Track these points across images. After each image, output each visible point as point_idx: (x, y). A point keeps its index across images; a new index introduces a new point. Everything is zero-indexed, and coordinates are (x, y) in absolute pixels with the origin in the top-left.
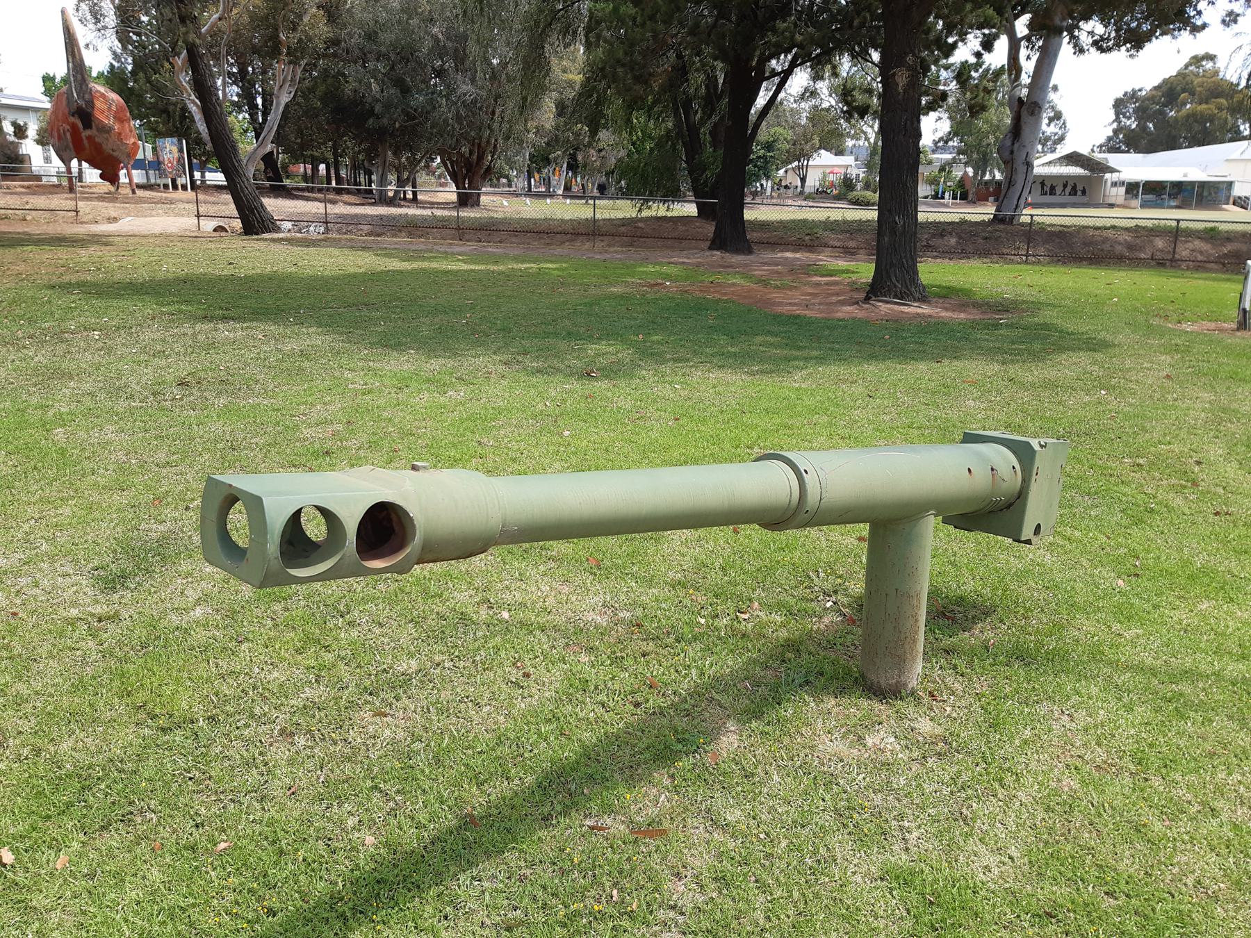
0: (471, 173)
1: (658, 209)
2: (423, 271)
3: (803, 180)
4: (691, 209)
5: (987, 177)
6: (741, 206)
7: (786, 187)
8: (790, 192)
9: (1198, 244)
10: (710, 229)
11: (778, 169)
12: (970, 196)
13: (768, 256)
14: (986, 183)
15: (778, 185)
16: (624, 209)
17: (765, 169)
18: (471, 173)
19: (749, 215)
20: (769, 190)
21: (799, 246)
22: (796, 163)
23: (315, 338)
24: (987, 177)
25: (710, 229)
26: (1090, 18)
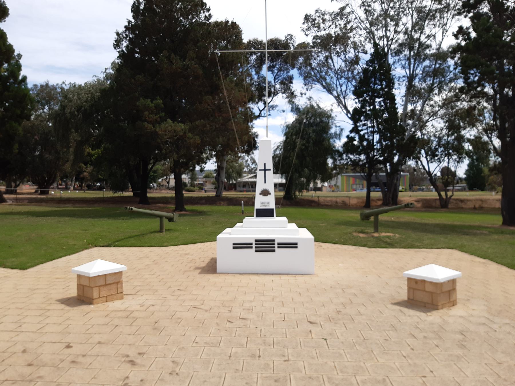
0: (43, 186)
1: (119, 194)
2: (66, 210)
3: (168, 183)
4: (131, 194)
5: (231, 182)
6: (146, 193)
7: (162, 186)
8: (164, 188)
9: (287, 352)
10: (138, 199)
11: (159, 179)
12: (227, 188)
13: (154, 205)
14: (231, 184)
15: (159, 185)
16: (109, 194)
17: (154, 180)
18: (43, 186)
19: (149, 195)
20: (156, 187)
21: (163, 203)
22: (165, 177)
23: (67, 219)
24: (231, 182)
25: (138, 199)
26: (393, 94)
